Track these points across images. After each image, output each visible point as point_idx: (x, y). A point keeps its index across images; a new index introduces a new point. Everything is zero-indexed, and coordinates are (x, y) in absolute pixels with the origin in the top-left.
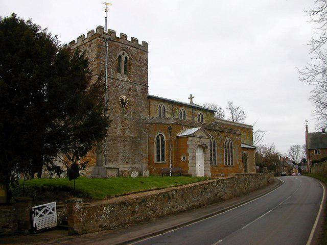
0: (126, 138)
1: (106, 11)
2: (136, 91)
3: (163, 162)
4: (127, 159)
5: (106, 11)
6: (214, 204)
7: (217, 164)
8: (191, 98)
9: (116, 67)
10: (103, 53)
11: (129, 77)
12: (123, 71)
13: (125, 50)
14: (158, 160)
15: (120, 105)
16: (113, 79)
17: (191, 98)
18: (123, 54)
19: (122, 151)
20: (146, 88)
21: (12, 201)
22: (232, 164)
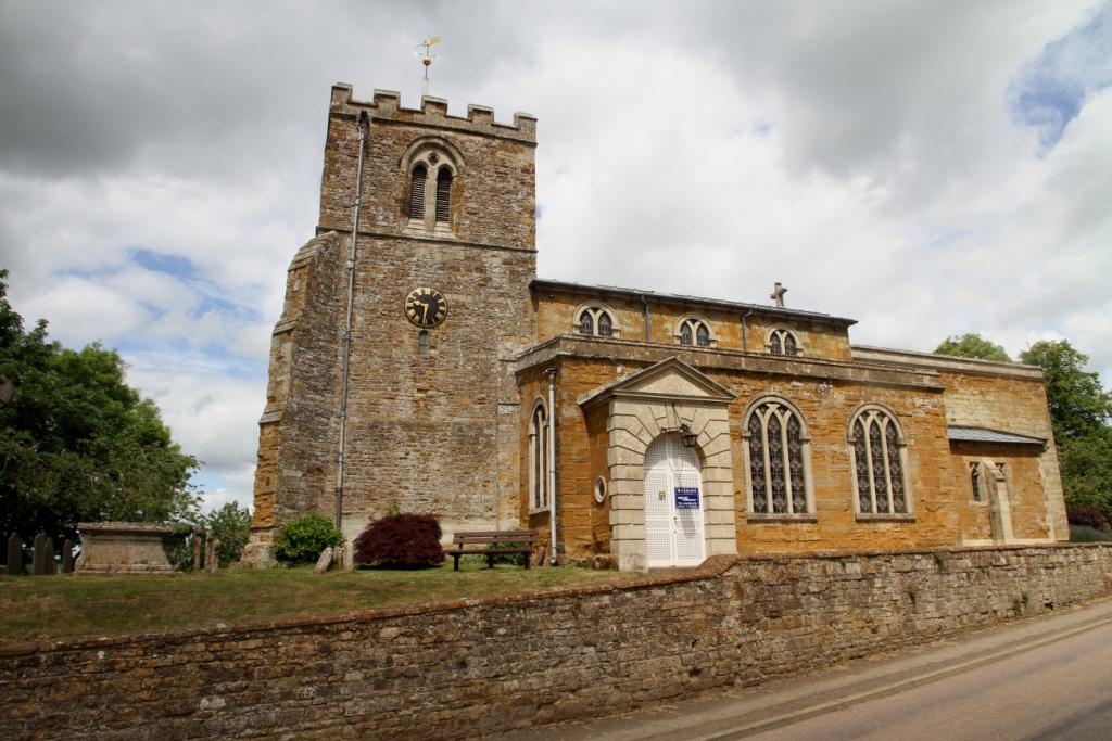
0: (431, 427)
1: (427, 63)
2: (481, 270)
3: (780, 516)
4: (436, 501)
5: (427, 63)
6: (873, 658)
7: (811, 509)
8: (780, 294)
9: (397, 201)
10: (343, 162)
11: (457, 228)
12: (430, 210)
13: (435, 146)
14: (538, 505)
15: (411, 320)
16: (382, 237)
17: (780, 294)
18: (433, 159)
19: (413, 474)
20: (526, 253)
21: (986, 570)
22: (901, 509)
